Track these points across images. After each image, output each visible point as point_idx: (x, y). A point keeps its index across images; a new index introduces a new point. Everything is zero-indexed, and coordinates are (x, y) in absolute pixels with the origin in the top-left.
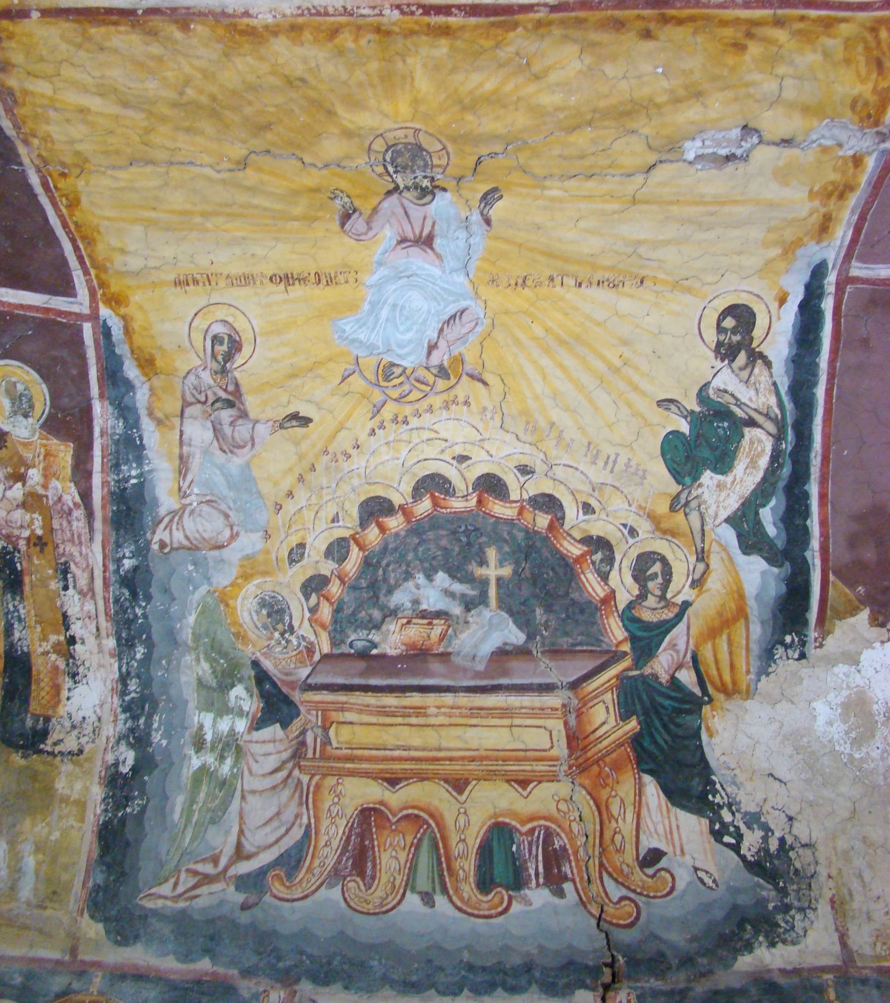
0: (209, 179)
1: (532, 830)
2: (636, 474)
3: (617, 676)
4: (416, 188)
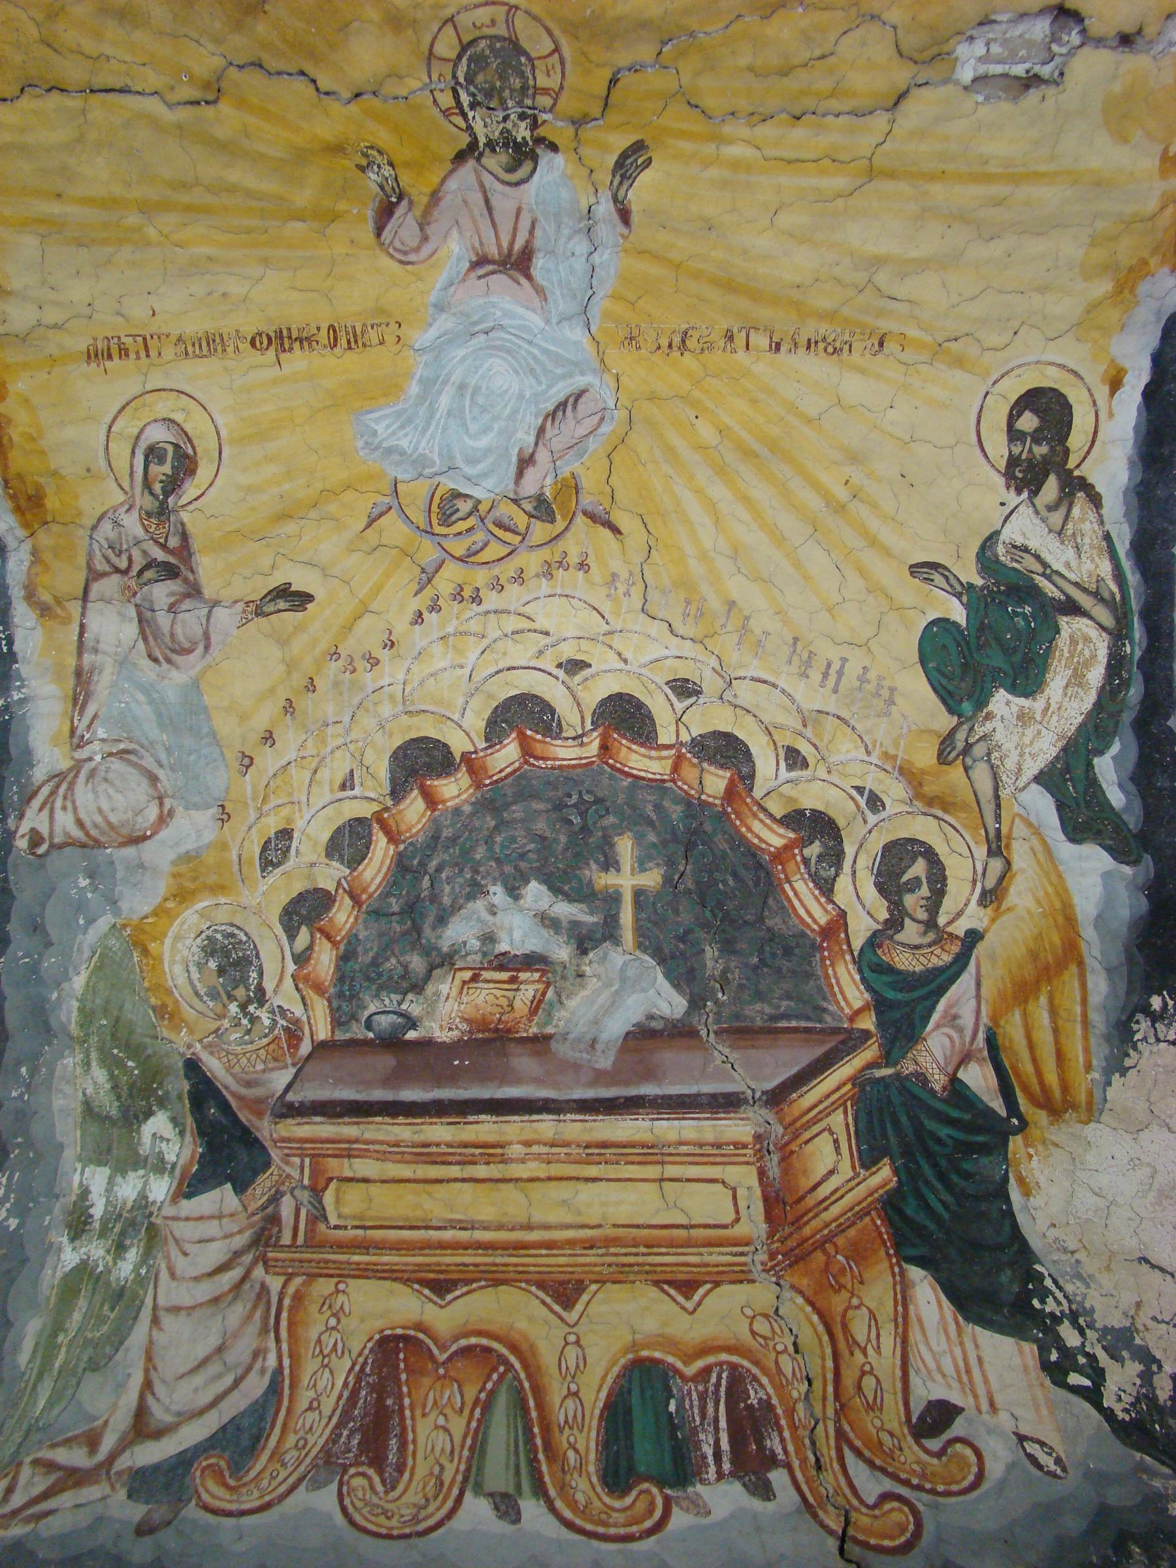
0: (155, 124)
1: (707, 1370)
2: (877, 694)
3: (853, 1079)
4: (506, 145)
